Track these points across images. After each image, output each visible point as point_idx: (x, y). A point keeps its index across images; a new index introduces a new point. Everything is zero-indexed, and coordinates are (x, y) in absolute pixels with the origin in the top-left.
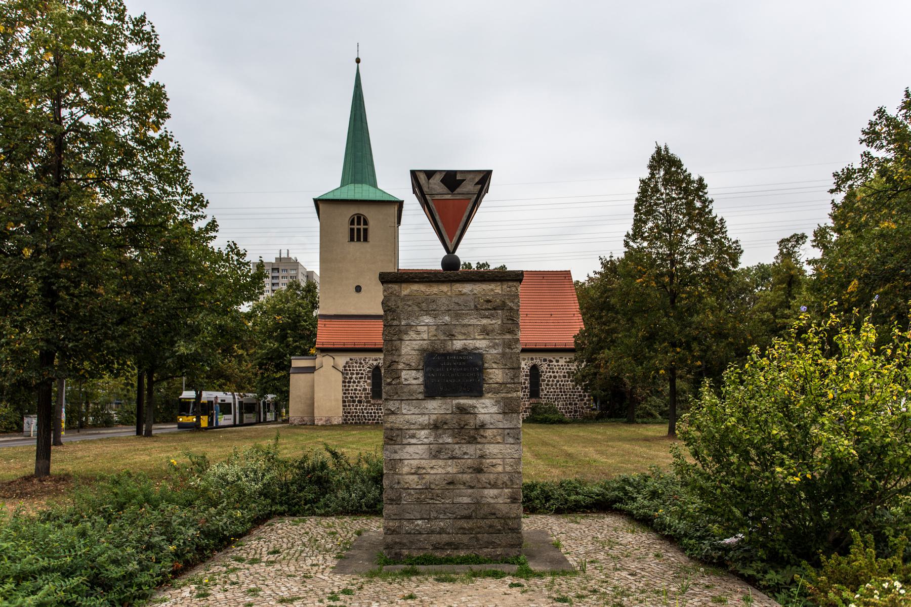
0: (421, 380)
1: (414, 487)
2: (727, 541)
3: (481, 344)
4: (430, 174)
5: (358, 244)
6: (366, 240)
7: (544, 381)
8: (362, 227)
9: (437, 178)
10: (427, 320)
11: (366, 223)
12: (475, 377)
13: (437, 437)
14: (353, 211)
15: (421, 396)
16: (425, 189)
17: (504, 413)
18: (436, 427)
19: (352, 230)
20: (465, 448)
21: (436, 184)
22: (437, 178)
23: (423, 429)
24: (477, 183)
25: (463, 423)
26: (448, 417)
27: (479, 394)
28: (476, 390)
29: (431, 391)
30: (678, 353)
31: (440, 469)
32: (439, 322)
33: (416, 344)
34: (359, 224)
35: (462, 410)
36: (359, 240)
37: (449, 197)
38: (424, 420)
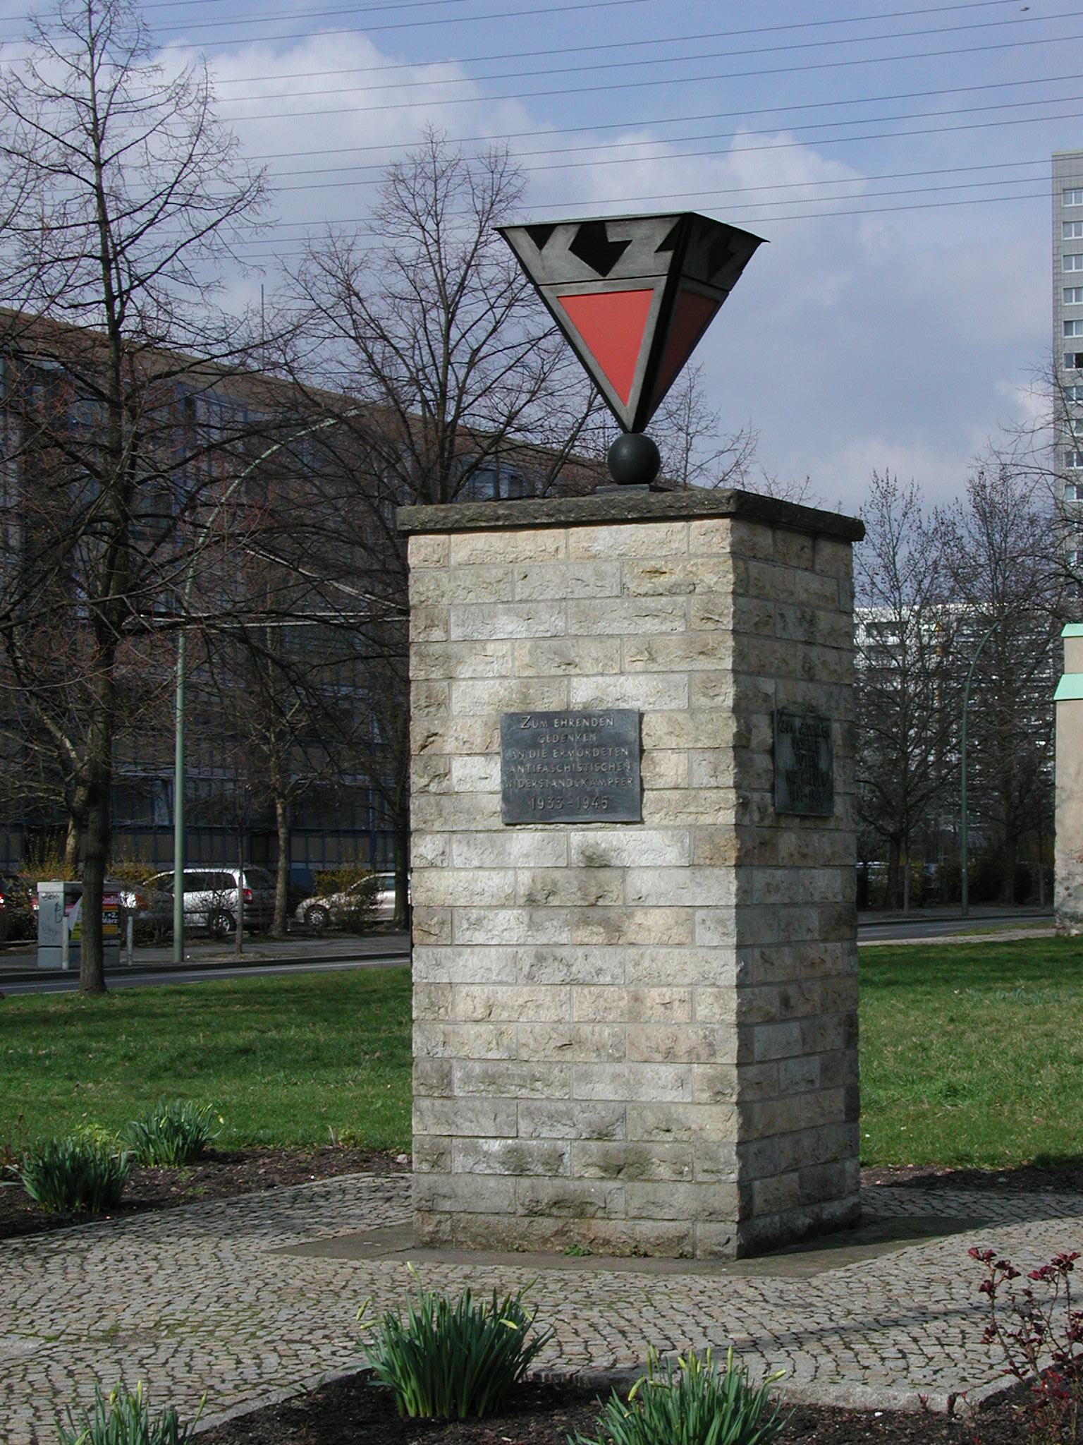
0: (496, 783)
1: (483, 1054)
2: (69, 848)
3: (631, 689)
9: (560, 243)
10: (508, 625)
12: (622, 773)
13: (533, 925)
15: (498, 823)
16: (535, 273)
18: (534, 901)
20: (599, 957)
22: (560, 243)
23: (502, 906)
24: (662, 248)
25: (594, 891)
26: (558, 875)
27: (635, 818)
28: (620, 801)
29: (522, 807)
30: (959, 730)
31: (539, 1012)
32: (540, 629)
33: (483, 690)
35: (595, 862)
37: (598, 287)
38: (494, 882)
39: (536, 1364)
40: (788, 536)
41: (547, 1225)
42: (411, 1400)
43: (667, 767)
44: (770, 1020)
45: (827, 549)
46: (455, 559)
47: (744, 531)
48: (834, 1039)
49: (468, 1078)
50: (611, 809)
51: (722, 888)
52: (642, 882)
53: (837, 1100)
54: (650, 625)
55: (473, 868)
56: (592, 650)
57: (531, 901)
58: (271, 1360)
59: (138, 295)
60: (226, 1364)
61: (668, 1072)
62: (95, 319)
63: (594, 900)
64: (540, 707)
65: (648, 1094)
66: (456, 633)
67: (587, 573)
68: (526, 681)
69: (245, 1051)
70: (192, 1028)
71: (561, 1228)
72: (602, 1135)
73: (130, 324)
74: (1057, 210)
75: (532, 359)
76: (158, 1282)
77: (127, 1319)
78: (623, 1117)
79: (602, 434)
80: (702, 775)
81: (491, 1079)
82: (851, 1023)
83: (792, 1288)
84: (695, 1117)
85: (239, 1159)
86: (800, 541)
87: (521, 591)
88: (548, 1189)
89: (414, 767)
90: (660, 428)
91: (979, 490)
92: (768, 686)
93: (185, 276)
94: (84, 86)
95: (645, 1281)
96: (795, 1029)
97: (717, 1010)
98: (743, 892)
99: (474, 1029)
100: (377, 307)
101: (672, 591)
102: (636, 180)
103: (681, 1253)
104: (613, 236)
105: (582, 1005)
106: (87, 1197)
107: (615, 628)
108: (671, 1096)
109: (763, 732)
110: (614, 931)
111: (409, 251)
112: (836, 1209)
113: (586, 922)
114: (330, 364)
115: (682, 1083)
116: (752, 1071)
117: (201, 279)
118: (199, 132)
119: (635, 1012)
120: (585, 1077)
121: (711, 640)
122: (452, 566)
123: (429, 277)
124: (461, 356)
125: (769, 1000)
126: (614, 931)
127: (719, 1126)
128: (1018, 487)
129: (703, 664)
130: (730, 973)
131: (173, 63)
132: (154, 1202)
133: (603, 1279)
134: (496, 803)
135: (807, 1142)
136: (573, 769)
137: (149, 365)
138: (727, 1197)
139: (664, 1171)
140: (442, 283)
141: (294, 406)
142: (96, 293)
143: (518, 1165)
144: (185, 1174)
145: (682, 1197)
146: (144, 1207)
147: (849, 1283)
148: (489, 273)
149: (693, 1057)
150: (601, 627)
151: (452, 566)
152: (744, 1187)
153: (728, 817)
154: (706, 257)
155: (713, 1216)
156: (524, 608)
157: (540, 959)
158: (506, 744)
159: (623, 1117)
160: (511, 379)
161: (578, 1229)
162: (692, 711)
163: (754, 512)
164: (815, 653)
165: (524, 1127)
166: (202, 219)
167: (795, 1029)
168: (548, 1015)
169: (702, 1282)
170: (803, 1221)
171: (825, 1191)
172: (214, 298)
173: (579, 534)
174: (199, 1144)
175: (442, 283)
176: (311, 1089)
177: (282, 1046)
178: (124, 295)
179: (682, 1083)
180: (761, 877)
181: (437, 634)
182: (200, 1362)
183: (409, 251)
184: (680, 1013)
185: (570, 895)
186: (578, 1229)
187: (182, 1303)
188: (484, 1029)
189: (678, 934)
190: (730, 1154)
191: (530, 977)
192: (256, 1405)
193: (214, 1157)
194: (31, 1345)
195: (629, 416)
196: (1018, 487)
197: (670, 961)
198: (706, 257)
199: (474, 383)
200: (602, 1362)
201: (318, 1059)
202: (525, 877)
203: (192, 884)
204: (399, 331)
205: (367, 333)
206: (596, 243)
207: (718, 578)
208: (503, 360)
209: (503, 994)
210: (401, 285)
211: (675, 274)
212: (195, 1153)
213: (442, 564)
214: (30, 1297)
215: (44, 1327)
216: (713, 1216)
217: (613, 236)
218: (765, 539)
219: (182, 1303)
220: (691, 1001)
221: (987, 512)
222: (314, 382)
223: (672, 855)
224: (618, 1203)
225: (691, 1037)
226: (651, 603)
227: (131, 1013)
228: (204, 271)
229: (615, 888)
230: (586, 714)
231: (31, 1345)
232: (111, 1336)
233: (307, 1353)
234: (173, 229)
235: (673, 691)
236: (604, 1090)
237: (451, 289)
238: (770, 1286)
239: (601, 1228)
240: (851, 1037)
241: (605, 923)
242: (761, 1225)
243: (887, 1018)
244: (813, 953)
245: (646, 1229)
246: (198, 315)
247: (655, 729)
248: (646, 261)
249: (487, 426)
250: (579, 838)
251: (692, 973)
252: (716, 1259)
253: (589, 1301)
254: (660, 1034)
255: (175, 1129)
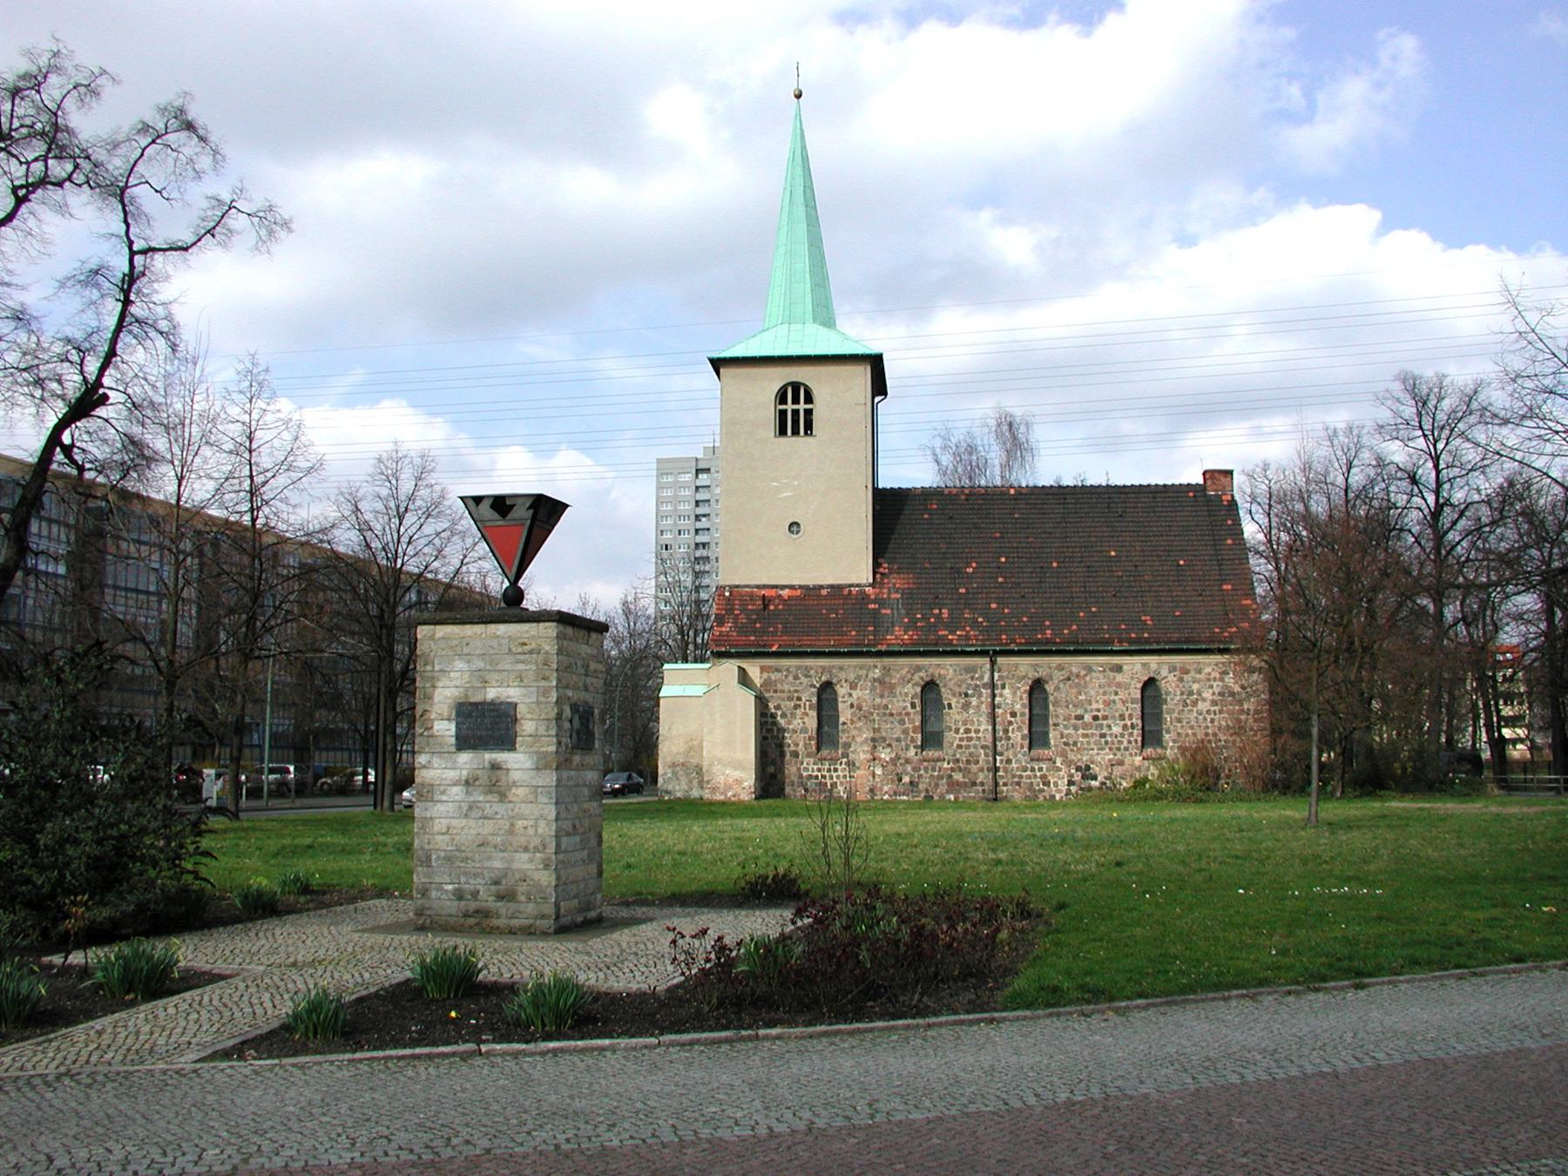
3: (512, 693)
4: (478, 500)
5: (795, 439)
6: (809, 426)
7: (1170, 712)
8: (802, 406)
9: (485, 505)
10: (460, 665)
11: (809, 400)
14: (779, 377)
15: (453, 749)
17: (537, 769)
19: (783, 414)
20: (496, 807)
21: (485, 507)
22: (485, 505)
29: (465, 742)
31: (469, 831)
33: (448, 692)
34: (796, 401)
35: (495, 767)
36: (796, 432)
38: (452, 774)
39: (481, 977)
40: (578, 627)
41: (472, 921)
42: (432, 991)
43: (527, 727)
44: (568, 834)
45: (594, 635)
46: (438, 635)
47: (561, 628)
48: (593, 842)
49: (438, 858)
50: (503, 743)
51: (550, 778)
52: (516, 776)
53: (593, 868)
54: (521, 667)
55: (442, 768)
56: (496, 676)
57: (467, 783)
58: (367, 975)
59: (266, 510)
60: (347, 976)
61: (525, 856)
62: (247, 518)
63: (494, 783)
64: (473, 700)
65: (515, 866)
66: (437, 668)
67: (494, 643)
68: (467, 689)
69: (310, 847)
70: (283, 836)
71: (479, 922)
72: (496, 883)
73: (261, 521)
74: (658, 482)
75: (437, 541)
76: (308, 942)
77: (300, 958)
78: (506, 875)
79: (497, 584)
80: (542, 731)
81: (448, 859)
82: (600, 836)
83: (580, 946)
84: (536, 876)
85: (324, 893)
86: (583, 633)
87: (466, 650)
88: (473, 905)
89: (418, 724)
90: (522, 584)
91: (625, 603)
92: (570, 693)
93: (285, 501)
94: (246, 418)
95: (517, 944)
96: (578, 839)
97: (547, 829)
98: (558, 780)
99: (440, 838)
100: (368, 516)
101: (531, 652)
102: (516, 474)
103: (529, 932)
104: (508, 502)
105: (488, 827)
106: (264, 909)
107: (507, 667)
108: (525, 867)
109: (567, 712)
110: (503, 797)
111: (384, 492)
112: (593, 914)
113: (491, 792)
114: (346, 541)
115: (531, 861)
116: (561, 856)
117: (293, 502)
118: (296, 438)
119: (511, 831)
120: (489, 858)
121: (547, 673)
122: (434, 638)
123: (392, 504)
124: (404, 539)
125: (567, 825)
126: (503, 797)
127: (547, 879)
128: (643, 603)
129: (544, 683)
130: (553, 815)
131: (285, 405)
132: (292, 910)
133: (499, 943)
134: (453, 741)
135: (582, 886)
136: (486, 726)
137: (268, 540)
138: (549, 909)
139: (522, 898)
140: (398, 507)
141: (329, 558)
142: (245, 507)
143: (459, 895)
144: (302, 899)
145: (530, 908)
146: (289, 912)
147: (603, 945)
148: (419, 503)
149: (536, 850)
150: (500, 667)
151: (434, 638)
152: (557, 905)
153: (553, 748)
154: (546, 511)
155: (543, 917)
156: (467, 657)
157: (470, 808)
158: (458, 715)
159: (506, 875)
160: (426, 550)
161: (485, 922)
162: (538, 703)
163: (564, 619)
164: (589, 680)
165: (463, 879)
166: (296, 476)
167: (578, 839)
168: (473, 832)
169: (541, 944)
170: (580, 919)
171: (588, 907)
172: (298, 510)
173: (492, 628)
174: (307, 886)
175: (398, 507)
176: (346, 863)
177: (328, 846)
178: (259, 508)
179: (531, 861)
180: (565, 774)
181: (429, 668)
182: (336, 975)
183: (384, 492)
184: (531, 831)
185: (484, 780)
186: (485, 922)
187: (322, 952)
188: (446, 838)
189: (531, 798)
190: (551, 890)
191: (466, 816)
192: (365, 993)
193: (313, 892)
194: (261, 968)
195: (512, 576)
196: (643, 603)
197: (526, 809)
198: (546, 511)
199: (410, 551)
200: (507, 975)
201: (344, 851)
202: (465, 773)
203: (272, 771)
204: (378, 527)
205: (364, 528)
206: (501, 504)
207: (550, 647)
208: (423, 541)
209: (455, 822)
210: (380, 506)
211: (534, 519)
212: (306, 889)
213: (432, 638)
214: (254, 949)
215: (264, 960)
216: (543, 917)
217: (508, 502)
218: (570, 631)
219: (322, 952)
220: (536, 826)
221: (627, 612)
222: (341, 549)
223: (529, 764)
224: (503, 911)
225: (536, 841)
226: (522, 657)
227: (254, 829)
228: (294, 497)
229: (504, 778)
230: (492, 703)
231: (261, 968)
232: (294, 964)
233: (381, 972)
234: (281, 480)
235: (528, 696)
236: (498, 864)
237: (402, 510)
238: (571, 945)
239: (495, 922)
240: (600, 842)
241: (499, 793)
242: (563, 921)
243: (611, 834)
244: (586, 806)
245: (515, 922)
246: (292, 519)
247: (522, 709)
248: (522, 513)
249: (416, 571)
250: (489, 756)
251: (537, 814)
252: (544, 935)
253: (496, 951)
254: (523, 840)
255: (297, 879)
